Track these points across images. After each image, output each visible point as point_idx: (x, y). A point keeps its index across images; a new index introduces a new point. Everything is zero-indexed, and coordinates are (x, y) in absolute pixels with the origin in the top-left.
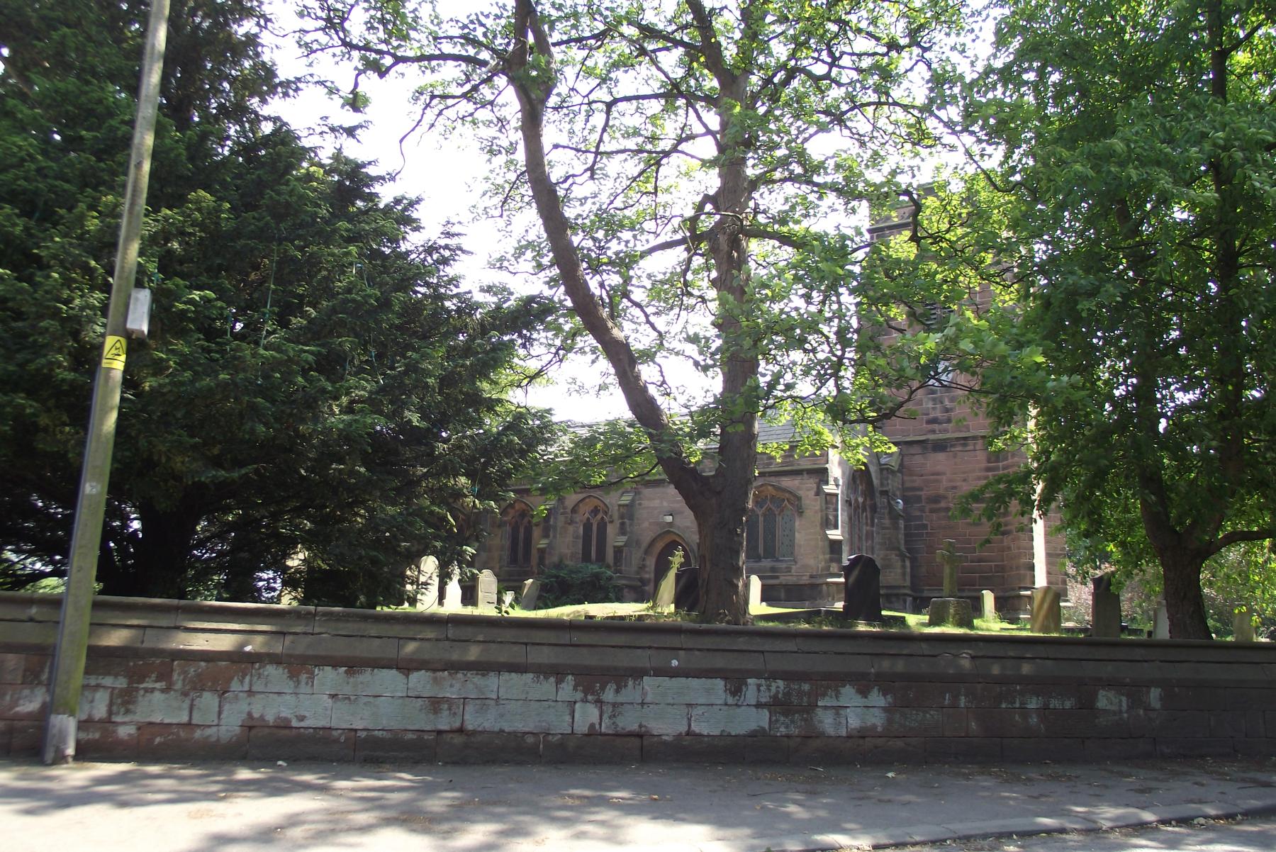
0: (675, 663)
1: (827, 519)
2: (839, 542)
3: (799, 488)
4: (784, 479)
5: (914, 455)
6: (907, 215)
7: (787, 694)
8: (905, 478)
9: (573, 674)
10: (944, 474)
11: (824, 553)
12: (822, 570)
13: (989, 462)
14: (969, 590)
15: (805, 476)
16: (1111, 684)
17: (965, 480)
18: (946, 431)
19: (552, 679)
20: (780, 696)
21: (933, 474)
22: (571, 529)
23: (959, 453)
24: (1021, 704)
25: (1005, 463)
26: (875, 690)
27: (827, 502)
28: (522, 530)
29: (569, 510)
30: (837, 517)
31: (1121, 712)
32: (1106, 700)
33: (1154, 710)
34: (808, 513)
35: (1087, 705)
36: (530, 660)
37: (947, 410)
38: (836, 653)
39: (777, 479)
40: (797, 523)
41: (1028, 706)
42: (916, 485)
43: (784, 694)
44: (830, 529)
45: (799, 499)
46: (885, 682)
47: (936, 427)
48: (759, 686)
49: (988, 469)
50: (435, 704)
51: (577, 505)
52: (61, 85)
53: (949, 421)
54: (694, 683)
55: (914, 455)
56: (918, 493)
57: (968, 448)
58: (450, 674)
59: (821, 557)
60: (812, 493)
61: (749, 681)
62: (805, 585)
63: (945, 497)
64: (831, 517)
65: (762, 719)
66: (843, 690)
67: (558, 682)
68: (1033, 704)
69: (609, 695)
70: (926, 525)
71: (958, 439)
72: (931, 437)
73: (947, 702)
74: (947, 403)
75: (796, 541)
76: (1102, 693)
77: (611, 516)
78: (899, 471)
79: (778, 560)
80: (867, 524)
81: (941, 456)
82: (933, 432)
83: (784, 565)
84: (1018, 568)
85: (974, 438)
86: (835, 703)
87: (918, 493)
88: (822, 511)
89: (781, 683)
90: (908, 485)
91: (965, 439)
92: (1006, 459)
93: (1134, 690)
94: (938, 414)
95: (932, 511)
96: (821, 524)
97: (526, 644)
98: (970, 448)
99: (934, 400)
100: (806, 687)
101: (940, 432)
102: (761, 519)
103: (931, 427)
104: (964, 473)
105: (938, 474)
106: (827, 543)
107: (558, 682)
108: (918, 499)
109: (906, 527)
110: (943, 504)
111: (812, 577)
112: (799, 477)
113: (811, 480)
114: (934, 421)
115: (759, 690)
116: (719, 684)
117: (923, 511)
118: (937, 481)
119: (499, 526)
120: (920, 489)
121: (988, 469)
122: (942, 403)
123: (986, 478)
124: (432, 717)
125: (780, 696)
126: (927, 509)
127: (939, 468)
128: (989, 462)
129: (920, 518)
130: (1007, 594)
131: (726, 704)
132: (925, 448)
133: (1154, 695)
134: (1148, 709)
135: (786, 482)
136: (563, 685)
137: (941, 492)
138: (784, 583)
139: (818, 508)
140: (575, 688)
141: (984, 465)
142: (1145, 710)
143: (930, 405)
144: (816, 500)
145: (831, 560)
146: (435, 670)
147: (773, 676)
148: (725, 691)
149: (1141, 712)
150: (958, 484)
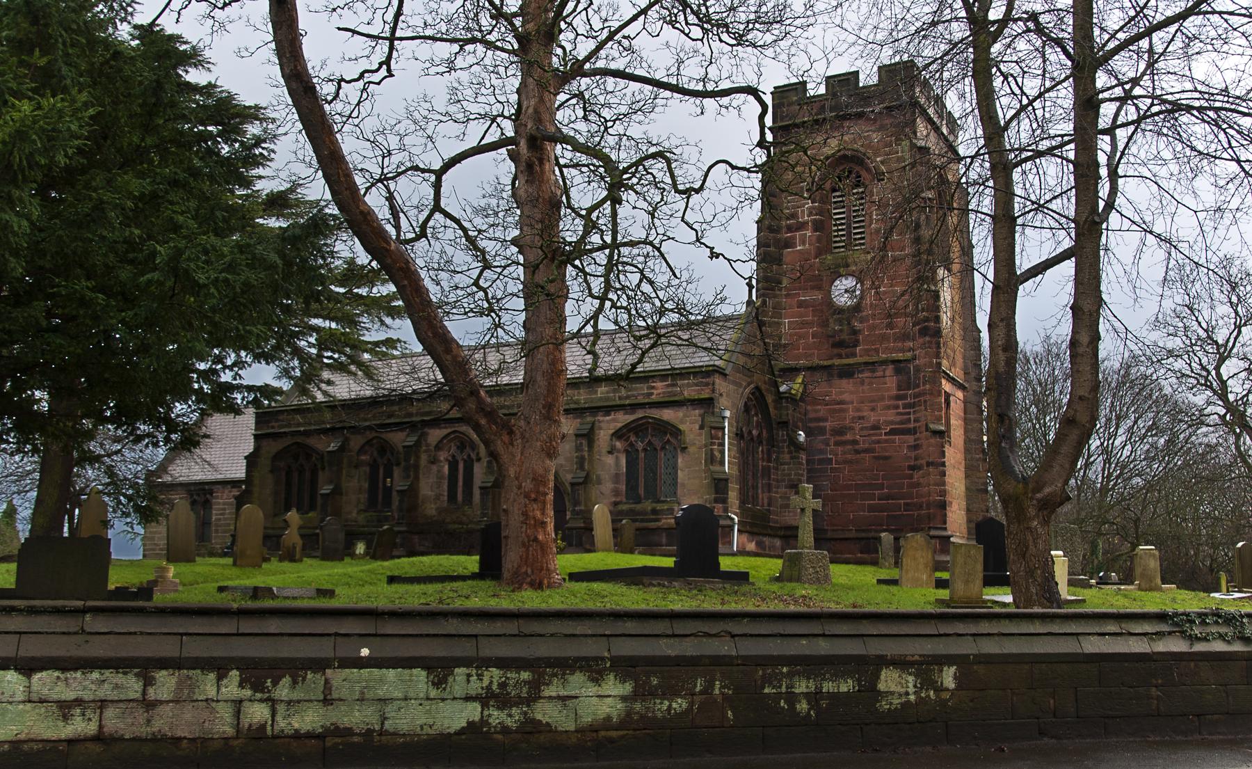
0: (365, 652)
1: (712, 455)
3: (682, 422)
7: (503, 685)
9: (238, 669)
13: (899, 390)
16: (901, 664)
17: (873, 409)
18: (854, 355)
19: (212, 676)
20: (495, 687)
21: (838, 404)
22: (434, 468)
24: (787, 688)
25: (916, 390)
26: (612, 677)
28: (461, 466)
29: (432, 448)
30: (723, 453)
31: (907, 694)
32: (889, 680)
33: (947, 690)
34: (692, 449)
35: (870, 691)
36: (185, 654)
38: (566, 635)
41: (797, 691)
42: (821, 414)
43: (499, 685)
46: (625, 667)
48: (469, 675)
49: (898, 398)
50: (65, 708)
51: (441, 441)
54: (391, 674)
56: (821, 424)
58: (83, 673)
61: (457, 670)
63: (852, 428)
64: (717, 453)
65: (473, 711)
66: (571, 678)
67: (220, 678)
68: (802, 686)
69: (283, 690)
71: (866, 364)
72: (837, 362)
73: (698, 689)
76: (884, 674)
77: (478, 454)
78: (802, 399)
79: (659, 501)
80: (763, 459)
81: (845, 384)
82: (840, 356)
85: (884, 362)
86: (563, 693)
87: (821, 424)
89: (495, 671)
91: (873, 363)
92: (918, 386)
93: (925, 668)
94: (845, 336)
95: (837, 444)
97: (182, 635)
98: (880, 374)
100: (525, 675)
102: (642, 455)
103: (836, 351)
104: (872, 401)
107: (220, 678)
108: (822, 431)
109: (807, 461)
110: (849, 437)
115: (468, 681)
116: (420, 674)
117: (828, 445)
119: (356, 467)
120: (826, 420)
121: (898, 398)
123: (897, 407)
124: (61, 724)
125: (495, 687)
126: (832, 443)
127: (846, 397)
128: (899, 388)
129: (822, 452)
131: (428, 699)
132: (831, 375)
133: (948, 678)
134: (940, 689)
135: (667, 414)
136: (225, 681)
140: (241, 686)
142: (935, 691)
144: (700, 435)
146: (64, 670)
147: (487, 663)
148: (427, 683)
149: (932, 693)
150: (865, 414)
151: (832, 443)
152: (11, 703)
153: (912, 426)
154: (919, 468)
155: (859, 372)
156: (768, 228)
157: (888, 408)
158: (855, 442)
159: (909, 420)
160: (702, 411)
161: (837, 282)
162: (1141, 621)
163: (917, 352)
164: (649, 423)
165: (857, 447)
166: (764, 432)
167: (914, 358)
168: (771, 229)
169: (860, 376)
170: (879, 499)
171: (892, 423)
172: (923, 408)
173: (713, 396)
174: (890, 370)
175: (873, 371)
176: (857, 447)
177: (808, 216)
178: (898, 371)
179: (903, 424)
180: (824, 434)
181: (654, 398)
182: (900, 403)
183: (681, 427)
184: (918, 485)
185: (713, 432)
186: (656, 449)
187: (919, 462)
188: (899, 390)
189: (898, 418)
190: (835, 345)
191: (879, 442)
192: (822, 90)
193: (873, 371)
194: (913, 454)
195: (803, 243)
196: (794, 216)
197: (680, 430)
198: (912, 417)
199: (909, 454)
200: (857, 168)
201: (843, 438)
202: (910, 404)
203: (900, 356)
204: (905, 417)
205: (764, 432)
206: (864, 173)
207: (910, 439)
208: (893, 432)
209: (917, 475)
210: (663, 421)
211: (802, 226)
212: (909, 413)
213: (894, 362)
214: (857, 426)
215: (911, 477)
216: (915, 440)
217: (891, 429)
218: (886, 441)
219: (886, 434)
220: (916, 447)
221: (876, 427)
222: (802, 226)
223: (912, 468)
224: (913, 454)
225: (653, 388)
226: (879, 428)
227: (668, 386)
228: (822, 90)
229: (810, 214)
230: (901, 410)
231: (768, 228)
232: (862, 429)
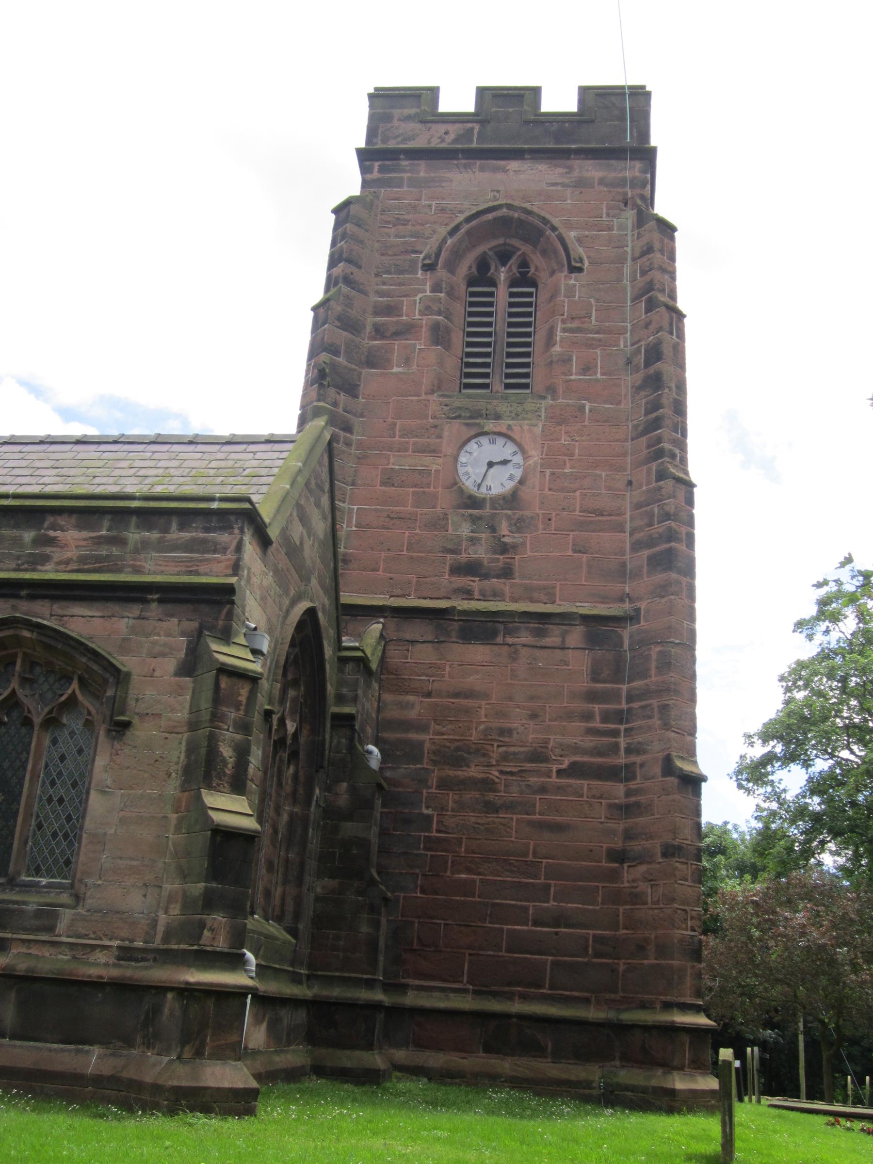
1: (212, 752)
2: (246, 838)
3: (124, 647)
4: (78, 609)
5: (413, 642)
6: (452, 136)
8: (388, 697)
10: (486, 696)
11: (184, 875)
12: (167, 937)
13: (595, 680)
14: (524, 997)
15: (154, 609)
17: (534, 716)
18: (497, 595)
21: (457, 695)
23: (524, 652)
27: (217, 699)
34: (142, 732)
37: (504, 549)
39: (57, 608)
40: (100, 762)
42: (413, 714)
44: (216, 789)
45: (120, 677)
47: (475, 584)
49: (592, 697)
52: (461, 1154)
53: (507, 573)
55: (413, 642)
56: (413, 736)
57: (548, 641)
59: (172, 886)
60: (170, 665)
62: (96, 985)
64: (227, 752)
70: (429, 818)
74: (504, 528)
75: (89, 824)
80: (295, 802)
81: (479, 652)
82: (468, 594)
83: (32, 902)
84: (662, 950)
85: (564, 618)
88: (193, 726)
90: (392, 713)
92: (645, 674)
94: (481, 553)
95: (445, 784)
96: (188, 771)
99: (474, 520)
101: (484, 598)
105: (469, 694)
106: (202, 839)
110: (474, 772)
111: (127, 954)
112: (136, 610)
113: (173, 623)
114: (471, 569)
118: (467, 711)
120: (423, 728)
121: (592, 697)
122: (493, 529)
123: (587, 716)
126: (434, 781)
127: (473, 681)
128: (595, 677)
130: (628, 1017)
137: (474, 736)
138: (22, 967)
139: (182, 715)
141: (584, 684)
143: (465, 530)
144: (179, 691)
145: (209, 902)
151: (434, 781)
152: (121, 858)
153: (621, 760)
154: (641, 858)
155: (508, 632)
156: (339, 319)
157: (570, 716)
158: (487, 785)
159: (616, 747)
160: (195, 625)
161: (472, 446)
162: (553, 1096)
163: (643, 605)
164: (19, 641)
165: (491, 796)
166: (305, 732)
167: (633, 618)
168: (349, 324)
169: (510, 640)
170: (536, 923)
171: (576, 749)
172: (656, 722)
173: (233, 580)
174: (576, 635)
175: (540, 633)
176: (491, 796)
177: (421, 313)
178: (593, 641)
179: (600, 754)
180: (418, 759)
181: (48, 573)
182: (597, 708)
183: (125, 662)
184: (636, 898)
185: (224, 682)
186: (27, 722)
187: (636, 846)
188: (595, 680)
189: (589, 742)
190: (457, 570)
191: (543, 789)
192: (469, 106)
193: (540, 633)
194: (620, 826)
195: (407, 361)
196: (390, 310)
197: (116, 671)
198: (623, 742)
199: (611, 825)
200: (525, 248)
201: (461, 774)
202: (621, 712)
203: (601, 610)
204: (606, 740)
205: (305, 732)
206: (537, 260)
207: (618, 790)
208: (575, 770)
209: (630, 875)
210: (66, 638)
211: (407, 330)
212: (615, 733)
213: (586, 619)
214: (496, 752)
215: (614, 876)
216: (628, 793)
217: (573, 765)
218: (560, 789)
219: (559, 772)
220: (628, 810)
221: (538, 756)
222: (407, 330)
223: (619, 857)
224: (620, 826)
225: (51, 542)
226: (546, 759)
227: (99, 541)
228: (469, 106)
229: (427, 310)
230: (597, 724)
231: (339, 319)
232: (505, 757)
